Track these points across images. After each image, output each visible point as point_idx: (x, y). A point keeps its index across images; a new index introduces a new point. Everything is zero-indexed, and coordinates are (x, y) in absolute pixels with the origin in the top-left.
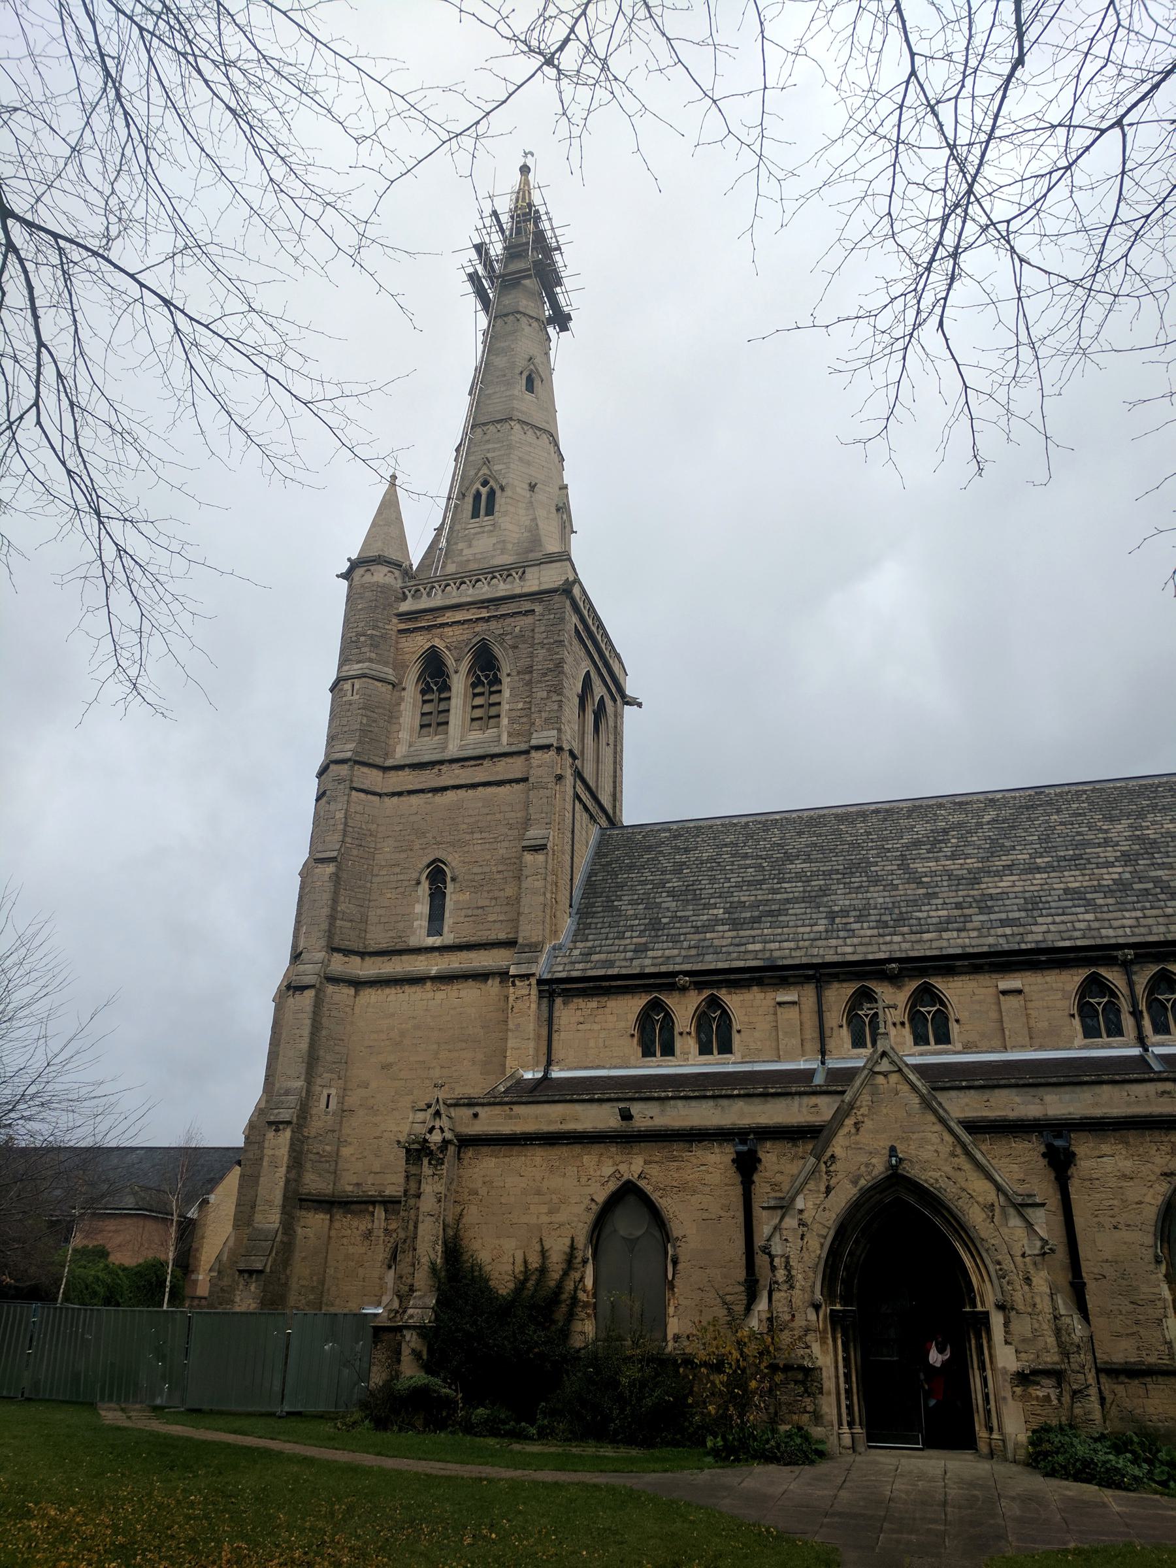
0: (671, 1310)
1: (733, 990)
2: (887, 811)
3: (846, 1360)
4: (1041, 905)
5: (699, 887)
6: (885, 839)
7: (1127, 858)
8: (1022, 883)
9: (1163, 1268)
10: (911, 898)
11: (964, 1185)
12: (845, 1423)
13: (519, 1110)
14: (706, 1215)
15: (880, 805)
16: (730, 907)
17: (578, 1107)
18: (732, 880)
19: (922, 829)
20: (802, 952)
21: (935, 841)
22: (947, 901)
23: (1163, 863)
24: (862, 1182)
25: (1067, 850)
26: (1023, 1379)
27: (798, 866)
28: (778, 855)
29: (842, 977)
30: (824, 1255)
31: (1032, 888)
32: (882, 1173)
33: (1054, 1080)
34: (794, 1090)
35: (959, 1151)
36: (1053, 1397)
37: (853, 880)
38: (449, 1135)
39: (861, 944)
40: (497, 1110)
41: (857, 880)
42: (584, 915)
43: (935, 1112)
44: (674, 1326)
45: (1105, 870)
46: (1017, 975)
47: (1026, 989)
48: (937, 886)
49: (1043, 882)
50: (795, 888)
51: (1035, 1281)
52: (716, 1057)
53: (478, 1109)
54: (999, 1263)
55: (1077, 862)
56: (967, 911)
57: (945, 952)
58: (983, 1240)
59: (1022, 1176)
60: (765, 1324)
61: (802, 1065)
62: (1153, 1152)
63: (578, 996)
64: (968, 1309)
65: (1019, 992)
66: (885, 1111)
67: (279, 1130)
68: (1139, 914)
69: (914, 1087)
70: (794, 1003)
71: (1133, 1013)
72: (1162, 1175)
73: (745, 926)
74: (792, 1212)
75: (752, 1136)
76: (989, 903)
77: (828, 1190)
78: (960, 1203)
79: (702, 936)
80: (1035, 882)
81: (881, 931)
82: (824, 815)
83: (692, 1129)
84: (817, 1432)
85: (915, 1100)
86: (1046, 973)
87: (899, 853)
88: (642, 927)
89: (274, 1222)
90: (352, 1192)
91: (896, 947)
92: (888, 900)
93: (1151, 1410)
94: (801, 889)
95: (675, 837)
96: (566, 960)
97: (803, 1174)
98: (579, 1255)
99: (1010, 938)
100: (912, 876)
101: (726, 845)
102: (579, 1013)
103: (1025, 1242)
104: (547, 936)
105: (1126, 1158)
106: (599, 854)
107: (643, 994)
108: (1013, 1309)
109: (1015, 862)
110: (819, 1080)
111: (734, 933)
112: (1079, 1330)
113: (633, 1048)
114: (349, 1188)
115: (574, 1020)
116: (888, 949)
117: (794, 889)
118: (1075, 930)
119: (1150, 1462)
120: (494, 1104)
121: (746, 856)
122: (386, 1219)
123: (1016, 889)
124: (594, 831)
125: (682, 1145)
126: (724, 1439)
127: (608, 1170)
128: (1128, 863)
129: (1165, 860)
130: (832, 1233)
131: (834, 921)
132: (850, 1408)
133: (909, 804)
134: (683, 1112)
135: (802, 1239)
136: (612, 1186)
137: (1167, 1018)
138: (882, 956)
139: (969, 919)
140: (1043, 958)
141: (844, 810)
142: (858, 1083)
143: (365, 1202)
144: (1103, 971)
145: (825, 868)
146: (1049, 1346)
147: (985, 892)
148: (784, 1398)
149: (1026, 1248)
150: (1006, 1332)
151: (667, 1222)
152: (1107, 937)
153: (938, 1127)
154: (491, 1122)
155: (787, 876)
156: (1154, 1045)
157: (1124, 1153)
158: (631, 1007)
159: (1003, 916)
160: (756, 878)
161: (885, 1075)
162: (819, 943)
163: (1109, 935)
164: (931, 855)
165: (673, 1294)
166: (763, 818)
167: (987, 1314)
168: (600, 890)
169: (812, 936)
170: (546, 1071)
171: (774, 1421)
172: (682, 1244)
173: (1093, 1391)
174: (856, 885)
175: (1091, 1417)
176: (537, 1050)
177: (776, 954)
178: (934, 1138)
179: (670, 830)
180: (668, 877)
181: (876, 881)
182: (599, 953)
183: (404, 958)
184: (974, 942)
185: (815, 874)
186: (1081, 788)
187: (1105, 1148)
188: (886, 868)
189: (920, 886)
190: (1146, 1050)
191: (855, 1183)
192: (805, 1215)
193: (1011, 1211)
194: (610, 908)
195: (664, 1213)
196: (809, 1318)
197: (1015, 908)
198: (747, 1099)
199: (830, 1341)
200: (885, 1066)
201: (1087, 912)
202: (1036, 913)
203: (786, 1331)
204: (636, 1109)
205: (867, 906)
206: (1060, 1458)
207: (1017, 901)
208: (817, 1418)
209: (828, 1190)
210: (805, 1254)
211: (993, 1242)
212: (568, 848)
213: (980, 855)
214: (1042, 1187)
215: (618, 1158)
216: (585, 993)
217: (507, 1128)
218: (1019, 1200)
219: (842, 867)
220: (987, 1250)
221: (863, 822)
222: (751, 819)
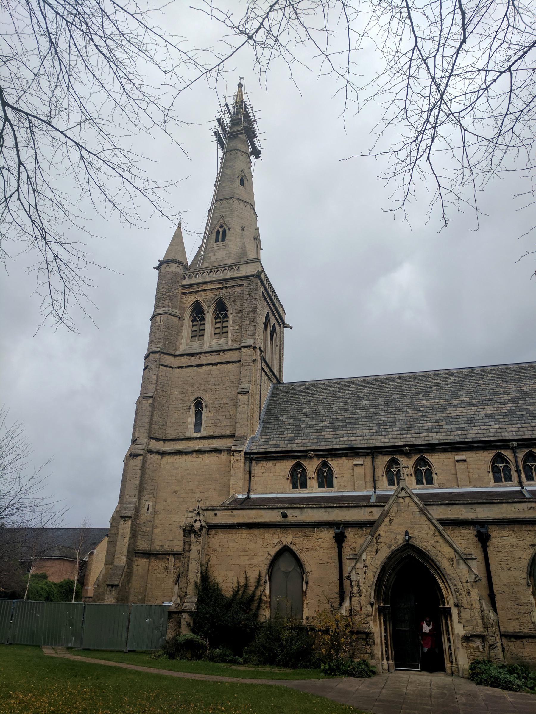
0: (305, 605)
1: (334, 459)
2: (404, 377)
3: (385, 629)
4: (474, 421)
5: (318, 411)
6: (403, 390)
7: (514, 400)
8: (466, 411)
10: (415, 417)
12: (385, 658)
13: (236, 512)
14: (321, 562)
15: (401, 375)
16: (333, 421)
17: (263, 511)
18: (333, 408)
19: (420, 386)
20: (365, 442)
21: (426, 392)
22: (432, 419)
23: (530, 403)
24: (393, 547)
25: (486, 396)
26: (467, 639)
27: (364, 402)
28: (355, 397)
29: (383, 453)
30: (375, 581)
31: (470, 413)
32: (402, 543)
33: (481, 501)
34: (361, 504)
35: (437, 533)
36: (480, 647)
37: (388, 409)
38: (203, 524)
40: (226, 512)
41: (391, 409)
42: (266, 423)
43: (426, 515)
44: (306, 613)
45: (503, 406)
46: (464, 453)
47: (468, 460)
48: (427, 412)
49: (475, 410)
51: (472, 594)
52: (326, 489)
53: (217, 512)
54: (456, 585)
55: (490, 402)
56: (440, 424)
57: (430, 442)
58: (448, 575)
59: (466, 545)
60: (348, 612)
61: (365, 493)
62: (526, 535)
63: (263, 460)
64: (441, 606)
65: (465, 461)
66: (403, 515)
67: (126, 521)
68: (519, 426)
70: (362, 465)
71: (517, 471)
72: (530, 545)
73: (339, 429)
74: (360, 561)
75: (342, 526)
77: (377, 551)
78: (438, 557)
79: (319, 434)
80: (472, 411)
81: (401, 432)
82: (376, 379)
83: (315, 522)
84: (372, 662)
85: (417, 510)
86: (477, 452)
87: (410, 397)
88: (292, 429)
89: (123, 563)
90: (159, 549)
91: (408, 440)
92: (404, 418)
93: (526, 654)
94: (365, 413)
95: (308, 388)
96: (257, 444)
97: (366, 543)
98: (263, 579)
99: (461, 436)
100: (416, 407)
101: (331, 392)
102: (263, 468)
103: (468, 576)
104: (249, 431)
106: (272, 396)
107: (293, 460)
108: (462, 606)
109: (463, 401)
110: (373, 500)
111: (334, 433)
112: (492, 616)
113: (288, 485)
114: (158, 548)
115: (261, 471)
116: (405, 441)
117: (362, 413)
118: (490, 432)
119: (526, 678)
122: (174, 562)
123: (463, 414)
124: (271, 385)
126: (329, 665)
127: (276, 541)
128: (514, 403)
129: (531, 401)
130: (379, 571)
131: (380, 428)
132: (387, 651)
133: (414, 374)
134: (311, 514)
135: (365, 573)
136: (278, 548)
138: (402, 444)
139: (441, 427)
140: (476, 445)
141: (384, 377)
144: (503, 452)
145: (376, 403)
146: (478, 624)
147: (449, 415)
148: (357, 646)
149: (468, 579)
150: (459, 617)
151: (303, 565)
152: (505, 436)
153: (428, 522)
154: (223, 518)
157: (513, 535)
158: (287, 465)
159: (457, 426)
160: (344, 407)
161: (403, 498)
162: (373, 437)
163: (506, 435)
164: (424, 398)
165: (306, 598)
166: (347, 380)
167: (450, 609)
168: (273, 412)
169: (370, 434)
170: (248, 495)
171: (352, 657)
172: (310, 575)
173: (499, 645)
174: (390, 411)
175: (499, 657)
176: (244, 485)
177: (354, 442)
178: (426, 528)
179: (305, 385)
180: (304, 406)
182: (273, 441)
183: (183, 442)
186: (492, 368)
187: (504, 533)
188: (404, 404)
189: (419, 412)
190: (523, 488)
191: (389, 547)
192: (367, 562)
194: (277, 420)
195: (302, 560)
196: (368, 610)
197: (463, 422)
198: (340, 508)
200: (403, 494)
201: (495, 425)
202: (472, 425)
203: (358, 616)
204: (289, 512)
205: (395, 421)
206: (484, 676)
207: (464, 419)
208: (372, 655)
209: (377, 551)
210: (366, 580)
211: (453, 575)
212: (258, 392)
213: (446, 398)
214: (475, 550)
215: (281, 535)
217: (230, 521)
218: (465, 556)
219: (383, 403)
220: (450, 580)
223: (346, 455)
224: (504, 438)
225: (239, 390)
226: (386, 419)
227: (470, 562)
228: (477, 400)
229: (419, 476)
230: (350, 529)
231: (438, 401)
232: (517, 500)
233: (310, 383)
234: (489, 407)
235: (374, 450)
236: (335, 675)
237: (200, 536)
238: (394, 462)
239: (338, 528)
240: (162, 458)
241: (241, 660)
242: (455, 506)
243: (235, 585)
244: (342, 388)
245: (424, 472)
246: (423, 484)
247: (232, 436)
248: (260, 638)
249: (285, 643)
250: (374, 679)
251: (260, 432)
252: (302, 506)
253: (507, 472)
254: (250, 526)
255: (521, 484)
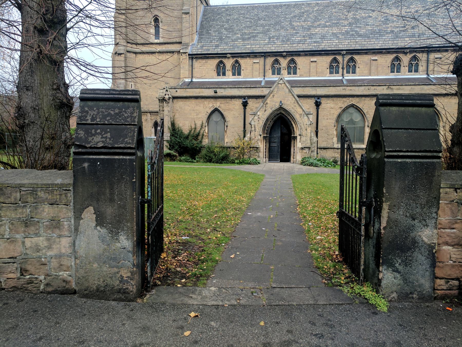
0: (226, 137)
2: (288, 5)
6: (286, 14)
8: (321, 30)
9: (335, 128)
10: (292, 33)
11: (296, 110)
13: (188, 90)
14: (235, 116)
17: (203, 90)
19: (297, 12)
20: (261, 49)
22: (301, 35)
24: (273, 109)
26: (302, 149)
27: (262, 22)
29: (271, 56)
30: (263, 125)
31: (324, 32)
33: (320, 85)
34: (257, 86)
35: (296, 102)
38: (170, 96)
39: (277, 47)
40: (182, 90)
42: (201, 34)
43: (291, 93)
44: (226, 140)
45: (343, 28)
46: (316, 57)
47: (317, 61)
48: (299, 30)
49: (327, 30)
50: (260, 29)
51: (308, 130)
52: (237, 76)
53: (177, 90)
55: (336, 25)
56: (306, 38)
59: (309, 108)
60: (249, 139)
61: (259, 79)
62: (339, 103)
68: (349, 41)
69: (287, 87)
70: (258, 63)
71: (342, 68)
73: (246, 40)
75: (246, 98)
76: (312, 36)
77: (265, 110)
79: (234, 43)
80: (325, 30)
84: (258, 159)
85: (287, 90)
88: (217, 39)
91: (286, 48)
92: (285, 34)
93: (327, 155)
95: (227, 10)
96: (196, 48)
97: (260, 107)
98: (204, 125)
99: (316, 47)
101: (241, 14)
102: (200, 64)
103: (307, 122)
104: (190, 40)
105: (333, 104)
106: (204, 15)
110: (263, 84)
111: (243, 42)
112: (315, 139)
113: (215, 74)
115: (199, 65)
118: (333, 45)
119: (324, 163)
120: (181, 88)
121: (247, 18)
123: (320, 32)
124: (202, 7)
125: (229, 99)
126: (239, 160)
127: (211, 105)
129: (360, 25)
130: (265, 120)
133: (294, 3)
134: (230, 91)
136: (212, 109)
137: (350, 69)
138: (282, 50)
140: (323, 53)
142: (274, 86)
143: (145, 112)
147: (312, 33)
148: (252, 153)
152: (340, 47)
153: (292, 97)
154: (181, 93)
155: (258, 25)
156: (345, 76)
158: (215, 62)
159: (315, 40)
161: (281, 84)
162: (266, 46)
163: (341, 47)
164: (298, 20)
169: (264, 44)
170: (192, 80)
171: (249, 158)
173: (316, 151)
176: (189, 74)
177: (254, 49)
178: (291, 99)
179: (225, 8)
180: (225, 24)
181: (282, 28)
182: (206, 47)
184: (306, 47)
185: (266, 25)
187: (328, 102)
190: (343, 78)
191: (271, 109)
192: (259, 116)
193: (305, 115)
194: (208, 33)
195: (225, 116)
197: (318, 38)
199: (263, 142)
200: (281, 82)
201: (336, 40)
202: (323, 40)
204: (218, 90)
205: (279, 36)
206: (307, 163)
207: (319, 36)
208: (259, 157)
209: (265, 110)
210: (259, 125)
212: (195, 13)
214: (313, 110)
215: (213, 102)
216: (201, 58)
217: (185, 95)
218: (307, 113)
221: (281, 8)
222: (249, 5)
223: (249, 57)
224: (340, 49)
225: (183, 11)
226: (274, 34)
227: (309, 116)
228: (329, 23)
229: (289, 70)
230: (250, 100)
231: (306, 23)
232: (338, 85)
233: (228, 6)
234: (335, 28)
235: (266, 54)
236: (242, 164)
237: (168, 103)
238: (277, 62)
239: (245, 99)
240: (136, 55)
241: (195, 161)
242: (306, 88)
243: (190, 128)
244: (248, 11)
245: (292, 68)
246: (291, 74)
247: (180, 43)
248: (204, 152)
249: (216, 153)
250: (259, 165)
251: (197, 40)
252: (225, 87)
253: (337, 69)
254: (196, 98)
255: (343, 75)
